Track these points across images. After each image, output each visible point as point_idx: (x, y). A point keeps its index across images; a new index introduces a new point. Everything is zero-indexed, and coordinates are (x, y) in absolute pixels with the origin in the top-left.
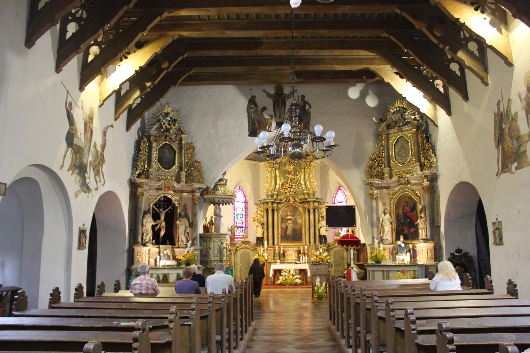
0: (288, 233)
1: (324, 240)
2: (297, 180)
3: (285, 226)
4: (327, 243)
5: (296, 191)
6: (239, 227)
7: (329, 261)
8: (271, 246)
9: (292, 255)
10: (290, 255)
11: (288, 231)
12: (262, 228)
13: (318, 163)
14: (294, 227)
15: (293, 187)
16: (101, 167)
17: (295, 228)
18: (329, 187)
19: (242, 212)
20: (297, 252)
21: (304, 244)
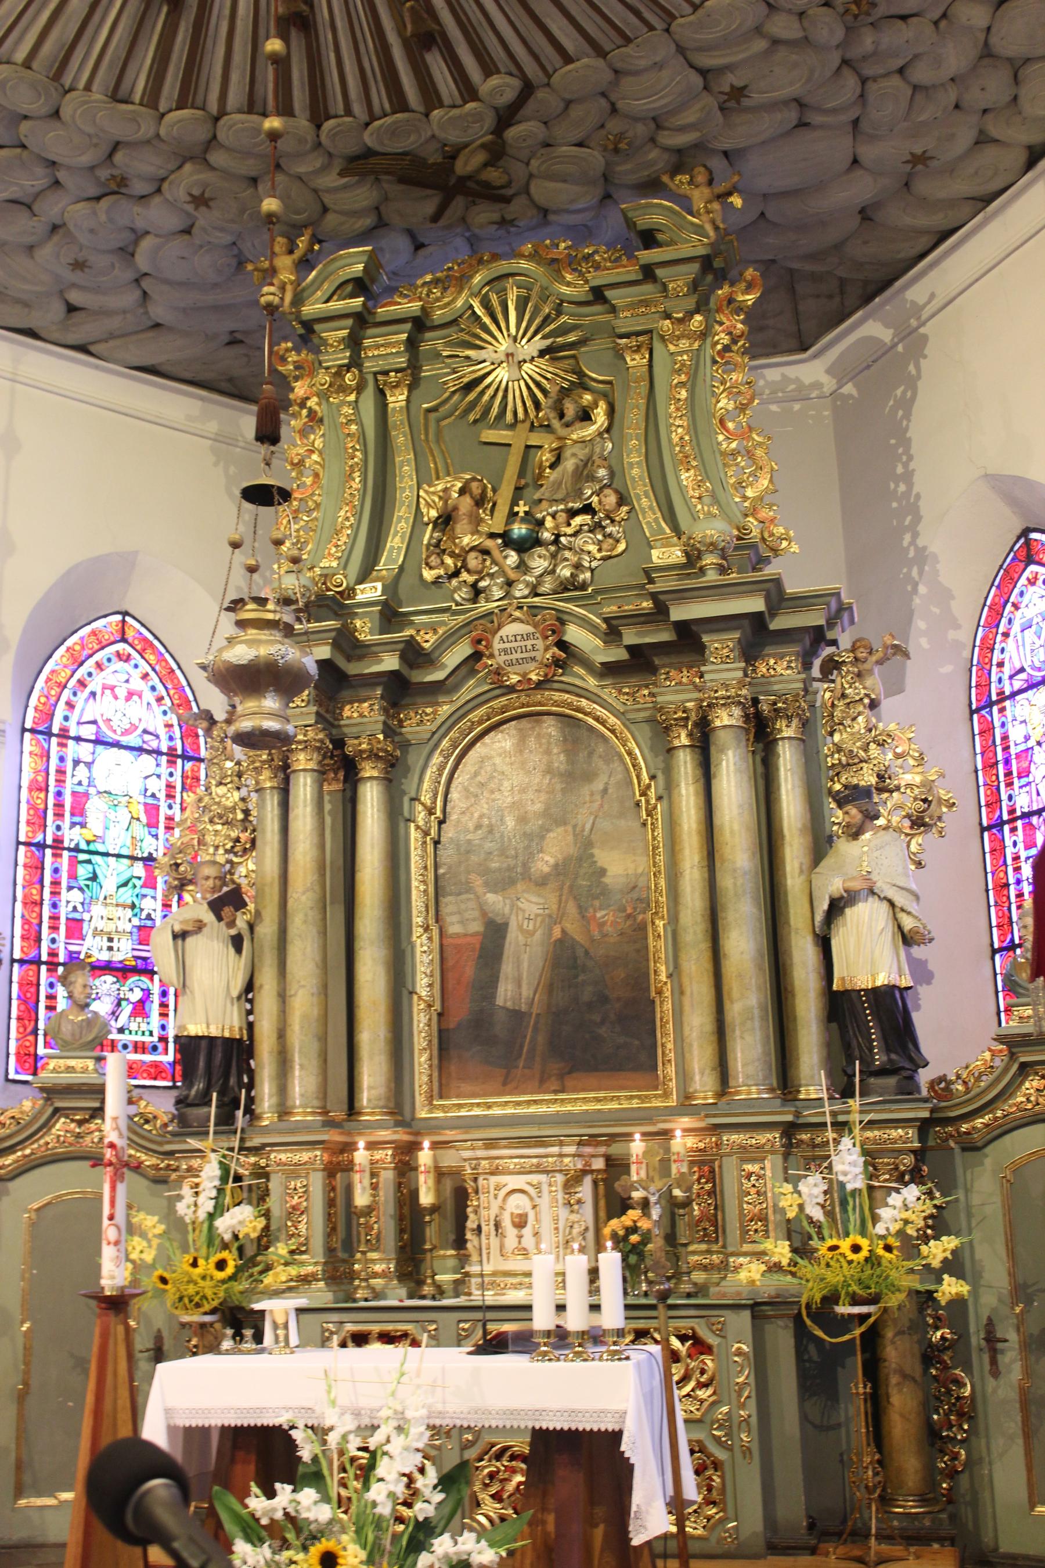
0: (505, 994)
1: (888, 1049)
2: (587, 462)
3: (476, 927)
4: (924, 1076)
5: (578, 566)
6: (106, 968)
7: (951, 1287)
8: (305, 1127)
9: (520, 1222)
10: (507, 1223)
11: (507, 968)
12: (237, 942)
13: (817, 385)
14: (573, 927)
15: (547, 536)
16: (911, 1046)
17: (578, 937)
18: (922, 557)
19: (140, 830)
20: (585, 1190)
21: (673, 1102)
